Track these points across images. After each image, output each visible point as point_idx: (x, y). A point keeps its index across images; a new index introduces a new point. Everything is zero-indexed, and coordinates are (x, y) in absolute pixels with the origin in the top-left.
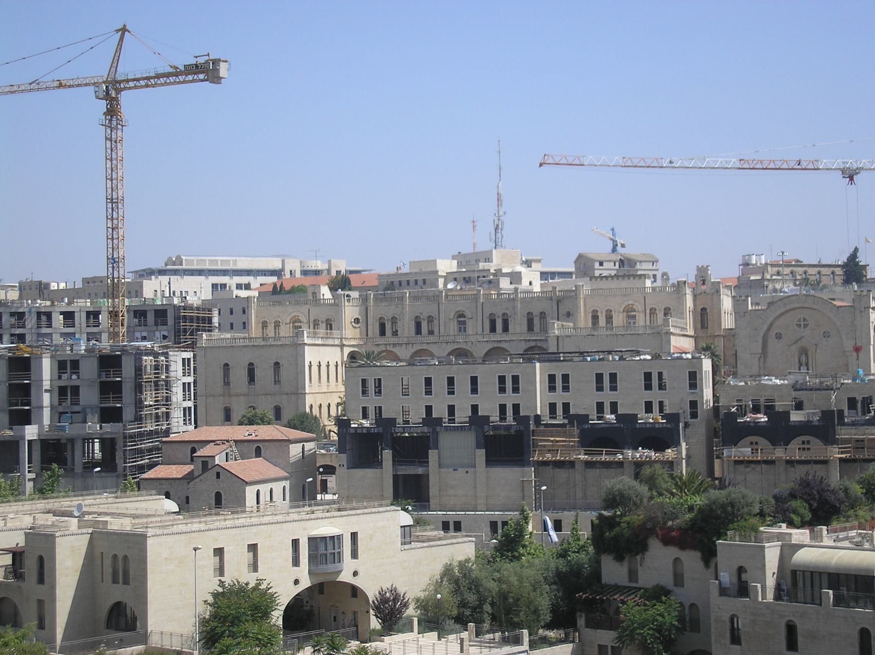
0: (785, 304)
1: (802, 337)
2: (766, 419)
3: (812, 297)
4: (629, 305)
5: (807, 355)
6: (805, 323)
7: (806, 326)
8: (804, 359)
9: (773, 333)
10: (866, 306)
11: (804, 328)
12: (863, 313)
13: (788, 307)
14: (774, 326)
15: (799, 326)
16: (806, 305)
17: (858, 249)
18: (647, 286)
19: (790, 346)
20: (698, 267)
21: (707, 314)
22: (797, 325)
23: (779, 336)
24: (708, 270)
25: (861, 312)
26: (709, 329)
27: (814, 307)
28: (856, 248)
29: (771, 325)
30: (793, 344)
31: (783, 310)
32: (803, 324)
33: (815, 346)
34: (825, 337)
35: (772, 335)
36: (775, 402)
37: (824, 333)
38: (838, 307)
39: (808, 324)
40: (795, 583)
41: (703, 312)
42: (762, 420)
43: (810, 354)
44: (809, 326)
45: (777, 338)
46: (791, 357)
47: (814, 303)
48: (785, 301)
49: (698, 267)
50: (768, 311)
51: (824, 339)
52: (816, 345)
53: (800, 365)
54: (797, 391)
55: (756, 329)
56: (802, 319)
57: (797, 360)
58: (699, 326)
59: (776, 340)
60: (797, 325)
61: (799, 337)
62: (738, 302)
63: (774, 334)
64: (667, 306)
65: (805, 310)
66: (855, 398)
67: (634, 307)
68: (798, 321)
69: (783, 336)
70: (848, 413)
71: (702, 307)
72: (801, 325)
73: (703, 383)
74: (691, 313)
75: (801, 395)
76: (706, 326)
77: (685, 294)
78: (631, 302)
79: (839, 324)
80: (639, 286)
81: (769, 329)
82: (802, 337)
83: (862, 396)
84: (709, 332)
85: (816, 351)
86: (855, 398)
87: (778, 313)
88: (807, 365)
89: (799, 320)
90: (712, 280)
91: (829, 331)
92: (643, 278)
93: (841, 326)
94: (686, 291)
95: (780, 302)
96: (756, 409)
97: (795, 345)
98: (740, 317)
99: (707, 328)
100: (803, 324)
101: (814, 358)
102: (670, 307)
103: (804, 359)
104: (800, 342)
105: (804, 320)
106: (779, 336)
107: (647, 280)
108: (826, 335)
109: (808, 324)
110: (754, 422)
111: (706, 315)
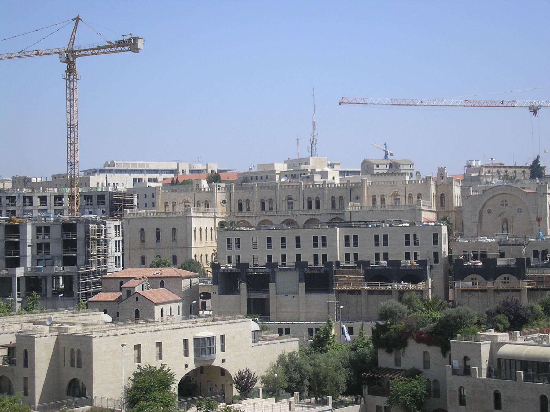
0: (494, 191)
1: (504, 212)
2: (482, 264)
3: (511, 187)
4: (396, 192)
5: (507, 223)
6: (506, 203)
7: (506, 205)
8: (505, 226)
9: (486, 210)
10: (544, 192)
11: (505, 206)
12: (542, 197)
13: (495, 193)
14: (486, 205)
15: (502, 205)
16: (507, 192)
17: (539, 157)
18: (406, 180)
19: (497, 217)
20: (439, 168)
21: (444, 197)
22: (501, 204)
23: (489, 212)
24: (445, 170)
25: (541, 196)
26: (446, 207)
27: (512, 193)
28: (538, 156)
29: (485, 204)
30: (498, 216)
31: (492, 195)
32: (505, 204)
33: (512, 218)
34: (518, 212)
35: (485, 211)
36: (487, 253)
37: (518, 209)
38: (527, 193)
39: (508, 204)
40: (499, 367)
41: (442, 196)
42: (479, 264)
43: (509, 222)
44: (509, 205)
45: (488, 213)
46: (497, 224)
47: (512, 191)
48: (494, 189)
49: (439, 168)
50: (483, 195)
51: (518, 213)
52: (513, 217)
53: (503, 229)
54: (501, 246)
55: (475, 207)
56: (504, 201)
57: (501, 227)
58: (440, 205)
59: (488, 214)
60: (501, 204)
61: (502, 212)
62: (464, 190)
63: (487, 210)
64: (419, 192)
65: (506, 195)
66: (538, 250)
67: (399, 193)
68: (502, 202)
69: (492, 211)
70: (533, 260)
71: (441, 193)
72: (503, 204)
73: (442, 241)
74: (434, 197)
75: (504, 248)
76: (444, 205)
77: (431, 185)
78: (396, 190)
79: (527, 204)
80: (402, 180)
81: (483, 207)
82: (504, 212)
83: (542, 249)
84: (446, 209)
85: (513, 221)
86: (538, 250)
87: (489, 197)
88: (507, 229)
89: (502, 201)
90: (448, 176)
91: (521, 208)
92: (404, 175)
93: (529, 205)
94: (431, 183)
95: (490, 190)
96: (475, 257)
97: (500, 217)
98: (465, 199)
99: (445, 206)
100: (505, 204)
101: (512, 225)
102: (421, 193)
103: (505, 226)
104: (503, 215)
105: (506, 201)
106: (489, 212)
107: (406, 176)
108: (519, 211)
109: (508, 204)
110: (474, 265)
111: (443, 198)
